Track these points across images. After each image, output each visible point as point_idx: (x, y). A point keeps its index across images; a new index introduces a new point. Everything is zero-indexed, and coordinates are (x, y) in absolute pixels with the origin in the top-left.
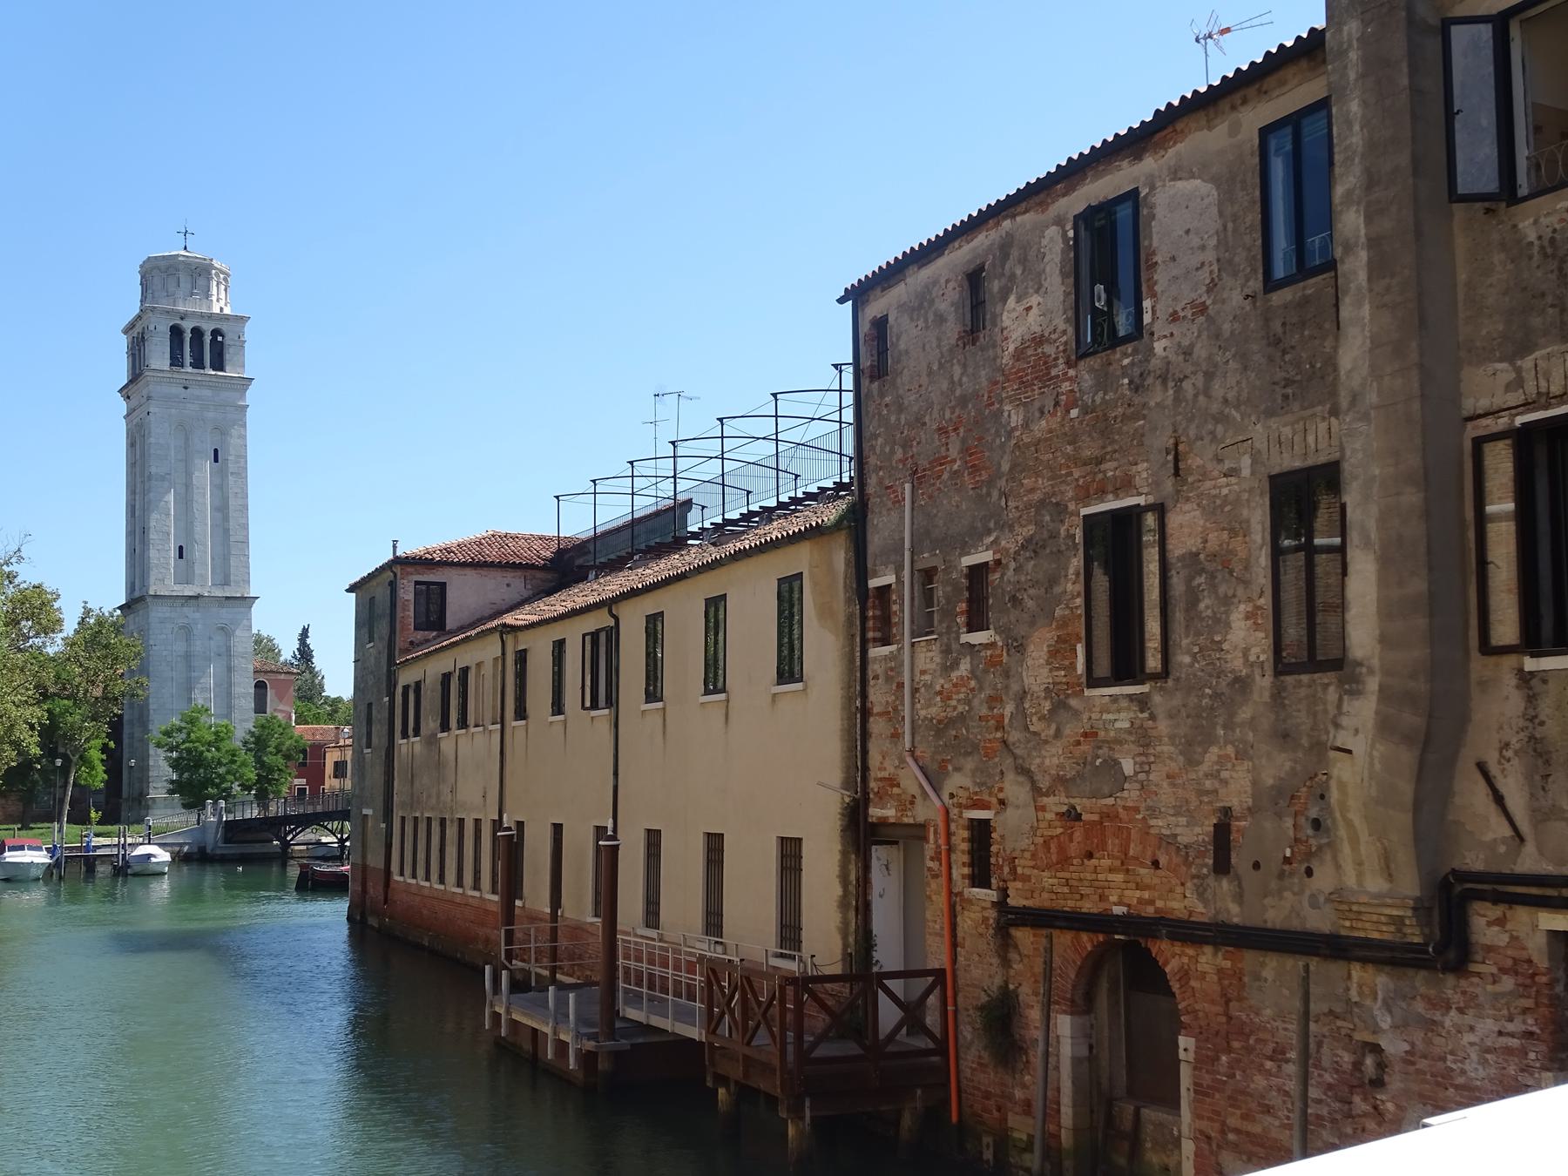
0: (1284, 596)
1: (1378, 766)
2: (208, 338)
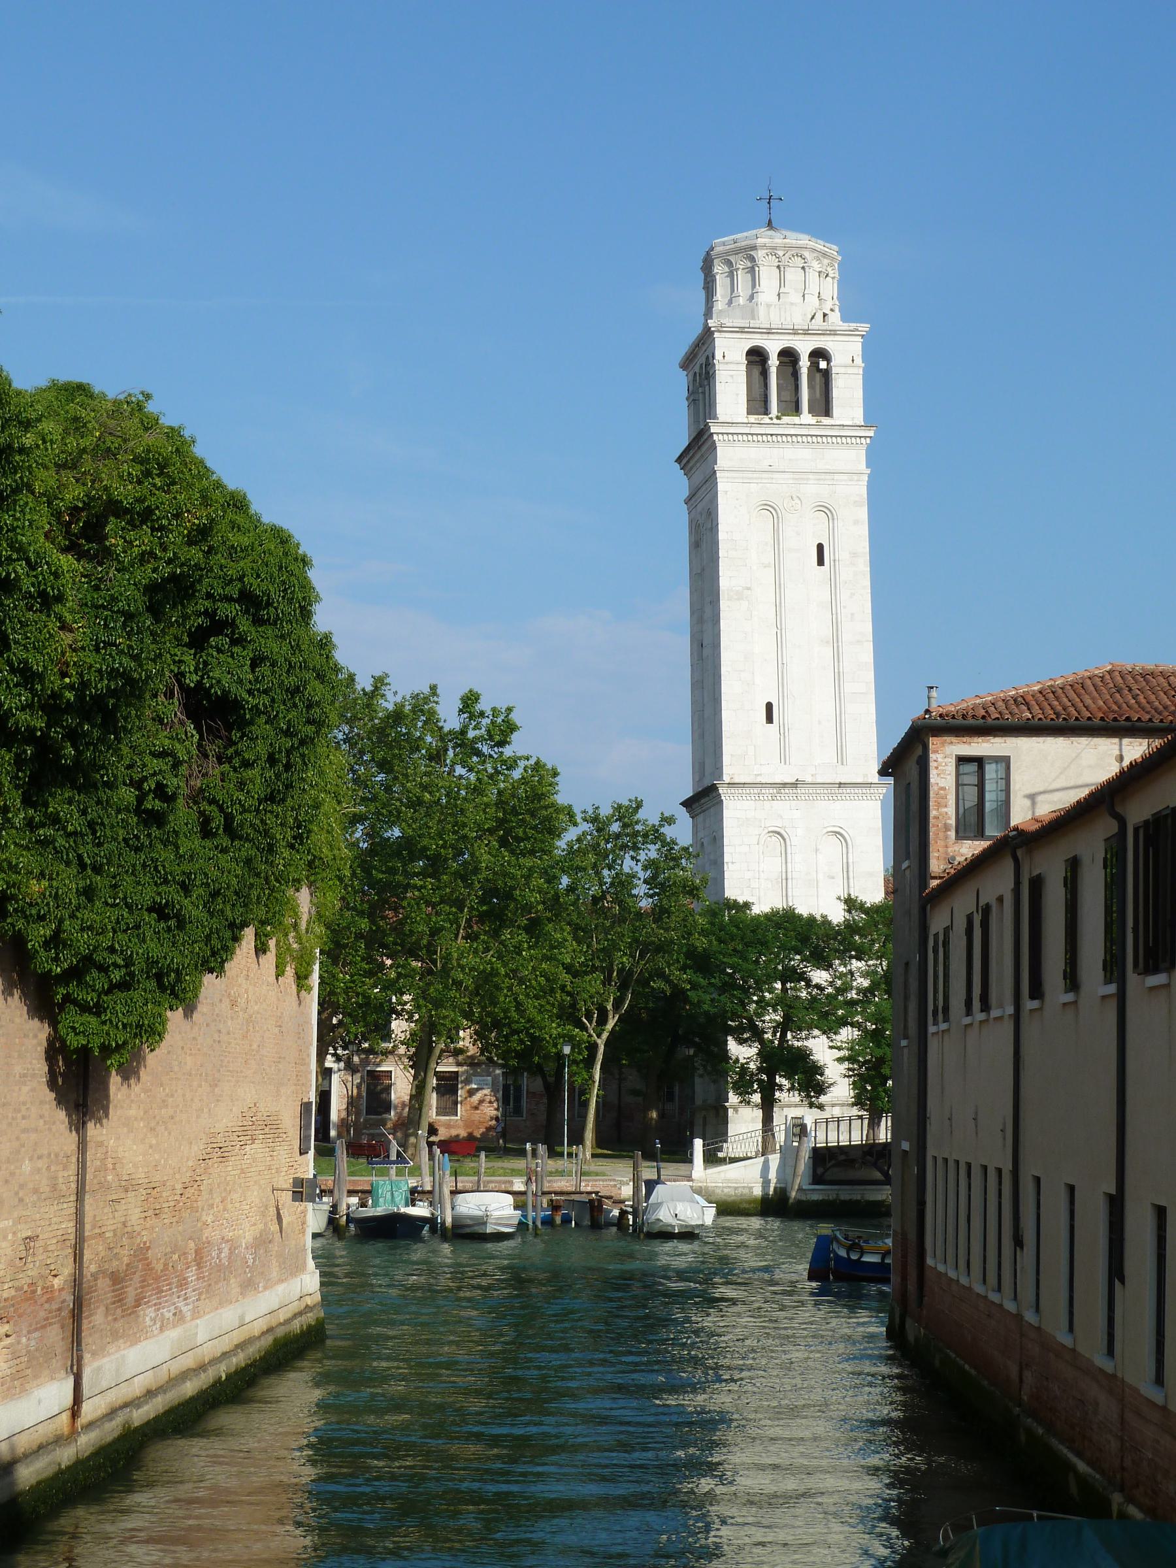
0: (1003, 1201)
2: (804, 363)
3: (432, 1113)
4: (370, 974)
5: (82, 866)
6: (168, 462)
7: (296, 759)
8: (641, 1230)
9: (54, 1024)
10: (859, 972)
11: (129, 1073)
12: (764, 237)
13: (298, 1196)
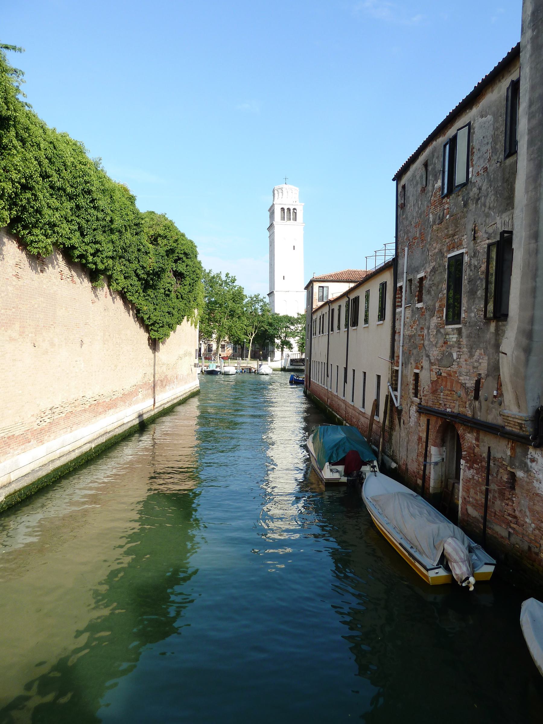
1: (514, 360)
2: (292, 211)
3: (220, 352)
4: (209, 326)
5: (154, 304)
6: (169, 227)
7: (194, 284)
8: (257, 373)
9: (149, 334)
10: (300, 327)
11: (163, 343)
12: (284, 186)
13: (195, 366)
